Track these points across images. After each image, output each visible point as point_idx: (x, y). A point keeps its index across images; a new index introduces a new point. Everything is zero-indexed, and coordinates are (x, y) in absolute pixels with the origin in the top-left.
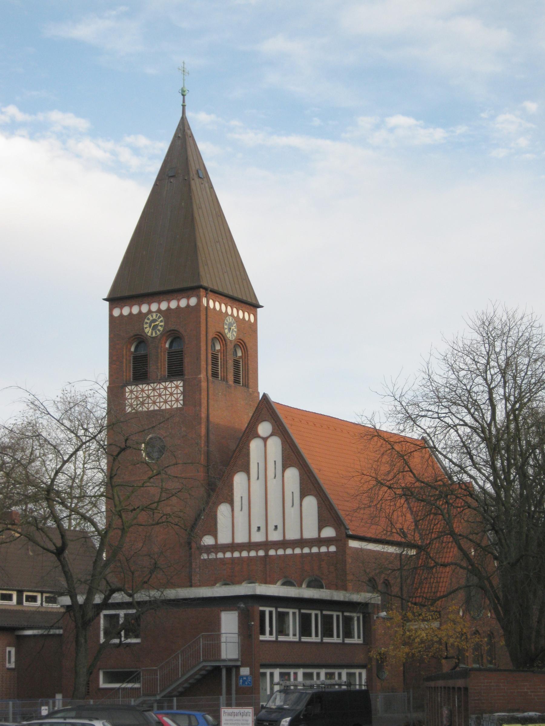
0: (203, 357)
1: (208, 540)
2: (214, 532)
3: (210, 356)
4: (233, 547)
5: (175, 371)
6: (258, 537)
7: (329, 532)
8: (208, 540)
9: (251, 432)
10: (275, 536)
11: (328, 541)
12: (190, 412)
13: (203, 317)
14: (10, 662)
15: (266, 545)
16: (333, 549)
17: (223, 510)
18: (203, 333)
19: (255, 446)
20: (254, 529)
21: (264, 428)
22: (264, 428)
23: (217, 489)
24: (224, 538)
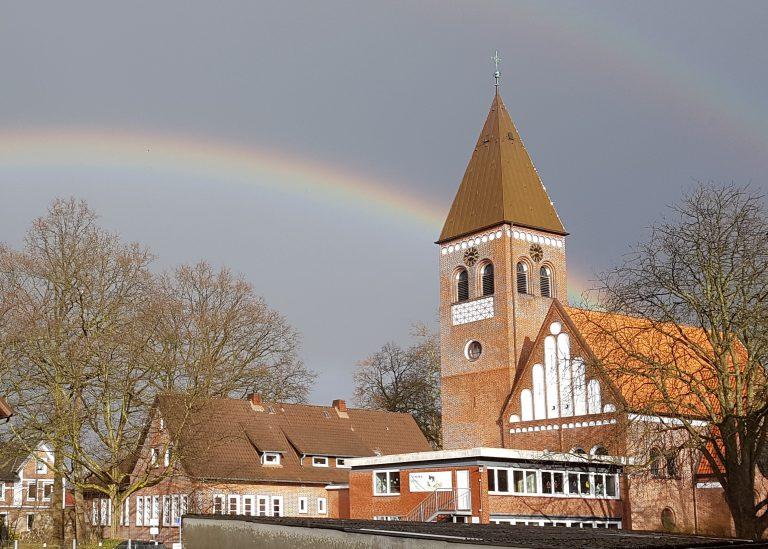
0: (509, 277)
1: (514, 419)
2: (518, 412)
3: (515, 276)
4: (535, 423)
5: (489, 290)
6: (553, 415)
7: (608, 408)
8: (514, 419)
9: (545, 331)
10: (566, 413)
11: (610, 416)
12: (502, 322)
13: (508, 246)
14: (302, 508)
15: (561, 420)
16: (613, 422)
17: (525, 395)
18: (508, 259)
19: (549, 342)
20: (550, 408)
21: (555, 328)
22: (555, 328)
23: (522, 376)
24: (527, 416)
